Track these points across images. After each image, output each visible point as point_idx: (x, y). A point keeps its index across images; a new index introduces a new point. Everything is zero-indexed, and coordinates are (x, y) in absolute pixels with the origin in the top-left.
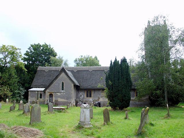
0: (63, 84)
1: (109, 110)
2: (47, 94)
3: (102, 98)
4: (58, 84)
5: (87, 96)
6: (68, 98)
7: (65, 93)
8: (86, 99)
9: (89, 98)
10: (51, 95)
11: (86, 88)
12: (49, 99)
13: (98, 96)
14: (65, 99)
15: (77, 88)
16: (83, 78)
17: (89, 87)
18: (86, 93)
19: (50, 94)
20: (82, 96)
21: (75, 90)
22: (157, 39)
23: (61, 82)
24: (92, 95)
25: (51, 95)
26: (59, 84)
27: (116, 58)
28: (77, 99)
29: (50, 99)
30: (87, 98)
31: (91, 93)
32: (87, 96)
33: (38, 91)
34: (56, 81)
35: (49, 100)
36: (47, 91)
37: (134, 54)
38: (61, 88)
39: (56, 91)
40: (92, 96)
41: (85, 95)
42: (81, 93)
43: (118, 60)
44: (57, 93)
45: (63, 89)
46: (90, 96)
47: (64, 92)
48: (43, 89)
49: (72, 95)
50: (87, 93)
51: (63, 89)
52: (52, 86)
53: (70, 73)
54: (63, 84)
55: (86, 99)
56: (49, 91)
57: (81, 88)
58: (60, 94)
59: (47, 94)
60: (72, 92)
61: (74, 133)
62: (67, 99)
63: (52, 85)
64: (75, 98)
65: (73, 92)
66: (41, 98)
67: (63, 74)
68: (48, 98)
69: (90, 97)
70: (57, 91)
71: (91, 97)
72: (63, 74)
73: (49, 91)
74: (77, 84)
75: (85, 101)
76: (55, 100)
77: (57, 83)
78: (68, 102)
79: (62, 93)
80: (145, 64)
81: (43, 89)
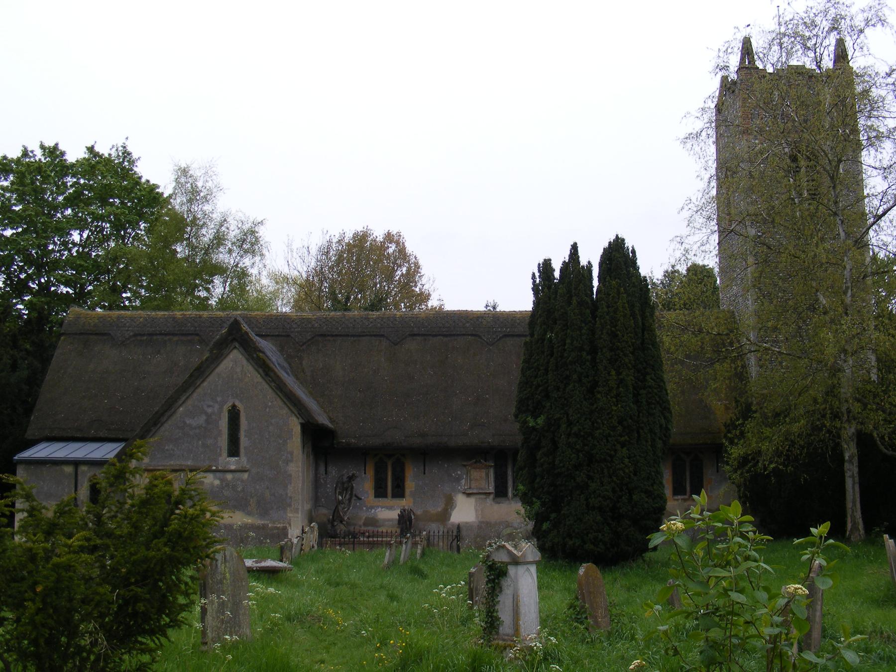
0: (234, 416)
1: (351, 478)
4: (201, 420)
7: (245, 476)
14: (249, 514)
15: (320, 442)
18: (371, 473)
21: (308, 456)
22: (782, 126)
23: (221, 408)
24: (410, 485)
26: (209, 416)
27: (575, 247)
31: (403, 471)
33: (76, 463)
37: (668, 220)
38: (223, 441)
40: (408, 492)
43: (583, 262)
45: (234, 451)
46: (399, 492)
49: (290, 488)
50: (377, 472)
51: (234, 451)
53: (265, 345)
54: (234, 416)
58: (217, 482)
62: (264, 509)
63: (166, 425)
65: (297, 467)
67: (234, 361)
69: (395, 496)
72: (234, 361)
74: (323, 419)
77: (205, 407)
78: (264, 527)
79: (229, 476)
80: (35, 304)
81: (107, 451)
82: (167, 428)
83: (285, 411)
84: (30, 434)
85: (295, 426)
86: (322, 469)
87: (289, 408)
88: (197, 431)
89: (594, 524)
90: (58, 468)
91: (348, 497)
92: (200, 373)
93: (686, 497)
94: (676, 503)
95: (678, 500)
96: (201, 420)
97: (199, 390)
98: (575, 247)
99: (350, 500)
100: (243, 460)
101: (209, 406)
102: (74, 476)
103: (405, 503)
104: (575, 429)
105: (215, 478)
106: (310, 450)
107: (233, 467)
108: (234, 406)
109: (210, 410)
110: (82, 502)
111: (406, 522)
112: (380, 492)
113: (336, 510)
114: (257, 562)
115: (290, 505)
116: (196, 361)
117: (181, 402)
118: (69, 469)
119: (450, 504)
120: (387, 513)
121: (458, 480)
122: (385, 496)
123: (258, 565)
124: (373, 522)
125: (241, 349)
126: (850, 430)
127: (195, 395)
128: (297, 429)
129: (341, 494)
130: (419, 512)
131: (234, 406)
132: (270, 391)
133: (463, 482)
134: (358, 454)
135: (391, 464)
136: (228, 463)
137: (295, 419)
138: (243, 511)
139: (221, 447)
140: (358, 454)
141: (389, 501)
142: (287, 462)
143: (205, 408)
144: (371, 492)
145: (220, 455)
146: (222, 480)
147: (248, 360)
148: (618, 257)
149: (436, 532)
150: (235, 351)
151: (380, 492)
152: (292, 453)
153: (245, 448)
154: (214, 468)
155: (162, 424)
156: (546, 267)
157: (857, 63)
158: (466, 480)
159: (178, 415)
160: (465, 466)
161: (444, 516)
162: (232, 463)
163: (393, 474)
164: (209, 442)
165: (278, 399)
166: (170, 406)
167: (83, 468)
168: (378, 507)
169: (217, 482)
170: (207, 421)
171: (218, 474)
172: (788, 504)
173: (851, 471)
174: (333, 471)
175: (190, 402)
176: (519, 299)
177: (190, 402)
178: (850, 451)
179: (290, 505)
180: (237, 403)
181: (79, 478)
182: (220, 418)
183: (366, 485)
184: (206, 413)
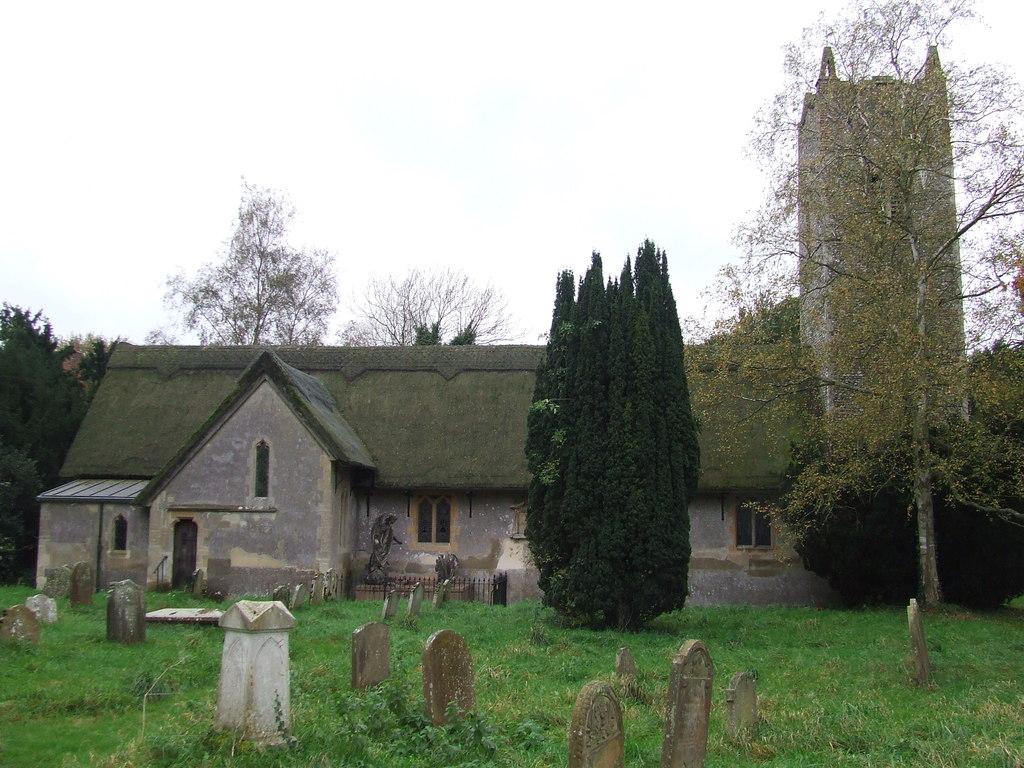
0: (263, 453)
1: (390, 520)
2: (162, 521)
7: (273, 517)
10: (185, 531)
15: (358, 482)
21: (344, 497)
24: (455, 528)
25: (185, 531)
26: (236, 452)
27: (597, 260)
31: (448, 512)
33: (102, 503)
38: (251, 480)
39: (215, 502)
40: (453, 536)
45: (262, 491)
46: (444, 536)
54: (263, 453)
56: (171, 499)
58: (244, 523)
59: (162, 521)
62: (291, 553)
64: (342, 550)
66: (120, 544)
67: (265, 394)
69: (438, 541)
72: (265, 394)
74: (360, 456)
77: (234, 443)
78: (291, 571)
79: (256, 517)
81: (132, 490)
82: (193, 466)
83: (316, 448)
84: (66, 470)
85: (326, 463)
86: (364, 511)
87: (320, 446)
88: (224, 469)
89: (615, 574)
90: (83, 507)
91: (385, 541)
92: (229, 406)
93: (751, 547)
94: (740, 553)
95: (742, 550)
96: (228, 457)
97: (228, 426)
98: (597, 260)
99: (388, 544)
102: (98, 517)
103: (445, 550)
104: (584, 469)
105: (242, 518)
106: (348, 489)
107: (261, 508)
108: (263, 443)
109: (237, 447)
110: (107, 543)
111: (445, 569)
112: (424, 536)
113: (373, 556)
114: (202, 612)
115: (319, 549)
116: (225, 394)
117: (208, 437)
118: (94, 509)
119: (496, 549)
120: (428, 557)
121: (506, 524)
122: (430, 541)
123: (203, 616)
124: (415, 568)
125: (271, 382)
126: (923, 476)
127: (223, 430)
128: (329, 467)
129: (377, 537)
130: (464, 558)
131: (263, 443)
133: (511, 526)
134: (405, 495)
135: (435, 505)
137: (326, 456)
139: (248, 486)
140: (405, 495)
141: (433, 545)
142: (317, 502)
143: (233, 443)
144: (415, 536)
147: (278, 394)
148: (650, 265)
149: (482, 579)
150: (265, 384)
151: (424, 536)
152: (321, 493)
153: (274, 487)
154: (241, 508)
155: (189, 461)
156: (565, 283)
157: (945, 58)
159: (204, 451)
161: (491, 562)
162: (260, 503)
163: (438, 513)
164: (237, 479)
165: (309, 435)
166: (199, 438)
167: (109, 508)
168: (422, 551)
169: (244, 523)
170: (236, 458)
171: (245, 515)
172: (859, 558)
173: (925, 521)
174: (375, 513)
175: (217, 438)
176: (527, 321)
177: (217, 438)
178: (922, 498)
181: (104, 517)
182: (248, 456)
183: (407, 527)
184: (235, 451)
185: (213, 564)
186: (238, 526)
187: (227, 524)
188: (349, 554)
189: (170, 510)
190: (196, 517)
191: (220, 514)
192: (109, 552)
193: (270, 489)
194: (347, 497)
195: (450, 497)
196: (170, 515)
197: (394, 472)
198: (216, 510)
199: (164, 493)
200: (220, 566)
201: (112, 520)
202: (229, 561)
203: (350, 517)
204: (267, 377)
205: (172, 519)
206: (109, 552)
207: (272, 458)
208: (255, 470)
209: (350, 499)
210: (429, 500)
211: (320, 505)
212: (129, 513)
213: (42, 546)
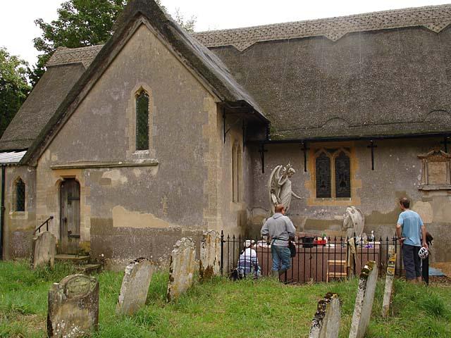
0: (143, 100)
2: (47, 181)
3: (427, 204)
4: (108, 110)
5: (323, 192)
6: (183, 203)
7: (155, 171)
8: (313, 209)
9: (333, 202)
10: (69, 188)
11: (308, 134)
12: (56, 214)
13: (400, 187)
16: (290, 77)
17: (335, 128)
18: (311, 169)
19: (62, 183)
20: (288, 191)
23: (128, 93)
24: (356, 183)
25: (69, 188)
28: (252, 208)
29: (68, 211)
30: (324, 202)
31: (348, 166)
32: (323, 192)
34: (96, 90)
35: (56, 221)
36: (49, 157)
38: (131, 132)
39: (96, 160)
40: (354, 190)
41: (309, 184)
42: (276, 171)
44: (108, 174)
45: (143, 144)
46: (344, 191)
47: (152, 160)
48: (17, 157)
49: (206, 184)
51: (143, 144)
52: (76, 121)
54: (143, 100)
55: (313, 209)
56: (55, 158)
57: (282, 136)
58: (124, 180)
59: (47, 181)
60: (207, 159)
61: (340, 178)
62: (175, 211)
64: (239, 207)
65: (218, 158)
66: (20, 207)
68: (51, 208)
69: (339, 196)
70: (106, 160)
71: (346, 194)
73: (55, 158)
74: (241, 94)
75: (307, 228)
76: (92, 220)
78: (53, 330)
79: (137, 172)
86: (259, 164)
100: (151, 151)
101: (116, 93)
105: (123, 174)
107: (141, 161)
115: (206, 205)
121: (413, 175)
125: (149, 25)
128: (213, 111)
131: (142, 91)
132: (181, 68)
134: (300, 147)
136: (136, 157)
137: (210, 99)
138: (153, 212)
140: (300, 147)
142: (202, 152)
144: (312, 193)
145: (127, 147)
146: (131, 177)
150: (143, 28)
158: (423, 175)
160: (420, 158)
162: (141, 156)
163: (338, 167)
179: (206, 205)
180: (144, 87)
185: (95, 224)
186: (119, 181)
187: (109, 181)
188: (245, 213)
189: (54, 169)
190: (79, 175)
191: (101, 170)
192: (11, 213)
193: (151, 141)
194: (239, 151)
195: (348, 149)
196: (54, 173)
197: (291, 117)
198: (98, 167)
199: (48, 151)
200: (101, 226)
201: (12, 182)
202: (111, 221)
203: (243, 173)
204: (143, 20)
205: (55, 178)
206: (11, 213)
207: (152, 107)
208: (135, 120)
209: (243, 154)
210: (346, 152)
211: (207, 155)
212: (25, 175)
213: (26, 200)
